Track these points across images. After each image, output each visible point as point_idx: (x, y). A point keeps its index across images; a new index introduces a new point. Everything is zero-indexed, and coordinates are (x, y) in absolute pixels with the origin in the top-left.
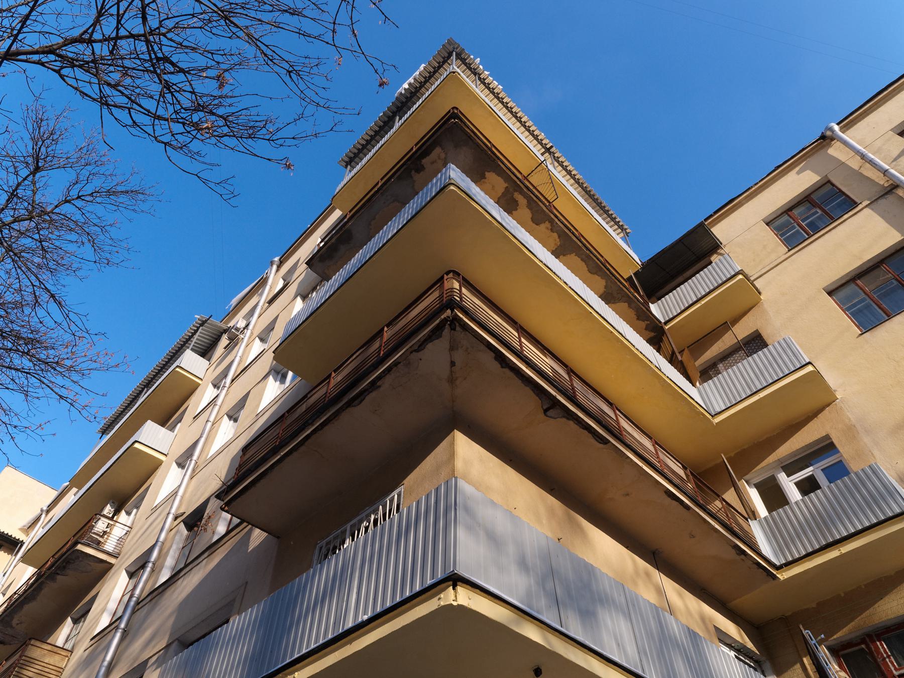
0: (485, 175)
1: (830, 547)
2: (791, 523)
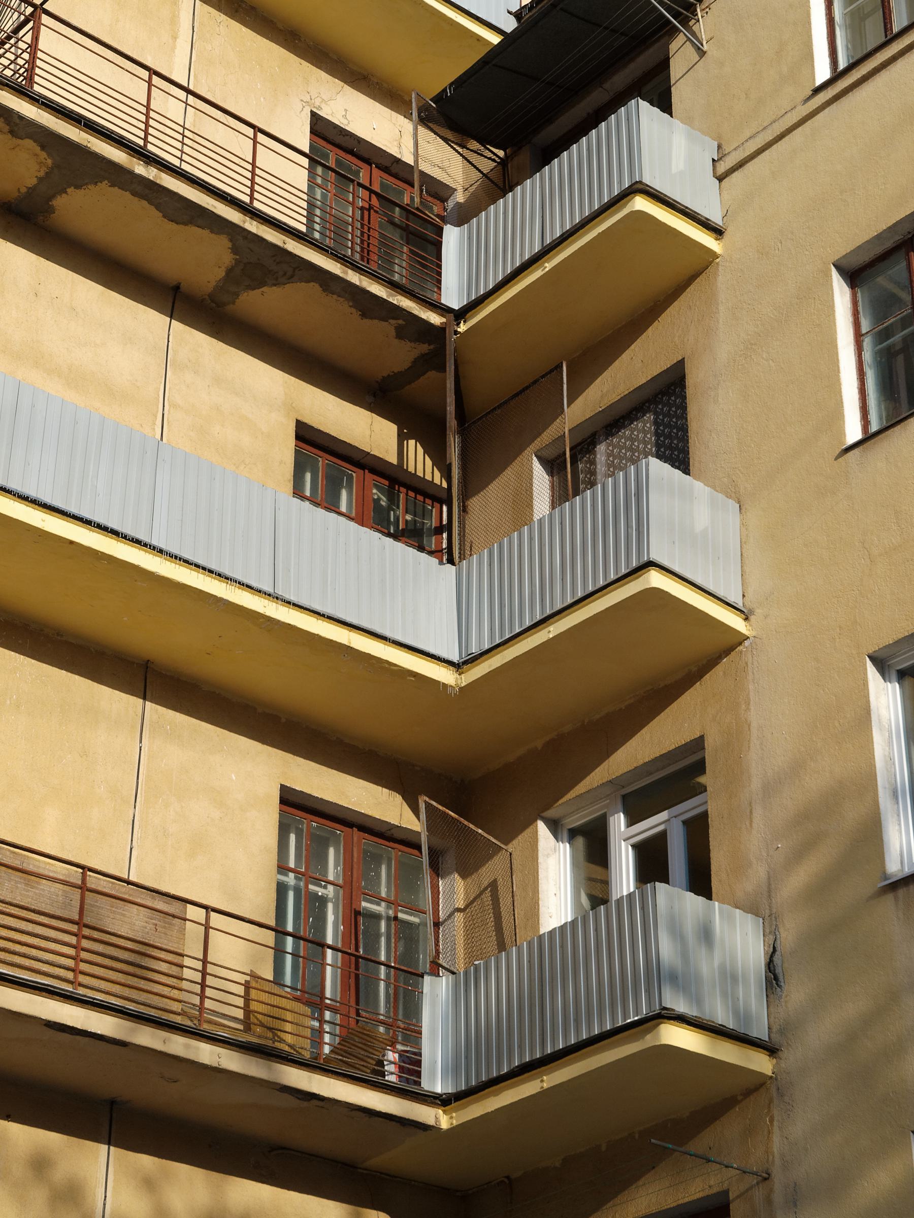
1: (529, 1071)
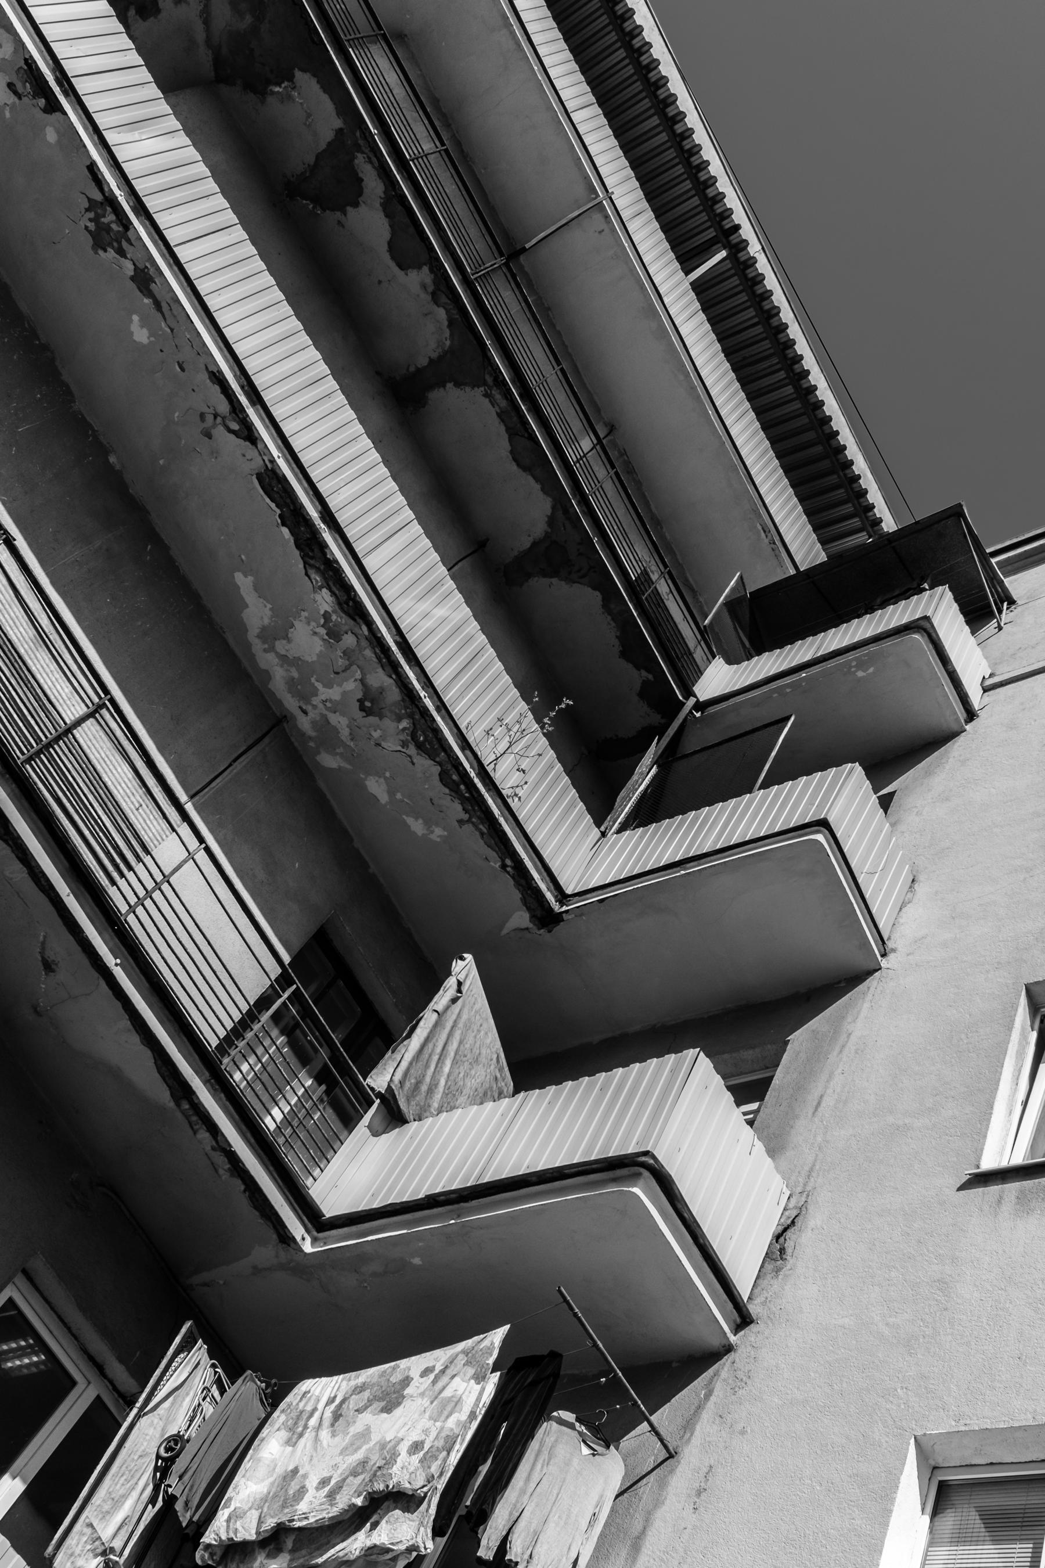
0: (329, 144)
2: (695, 256)
